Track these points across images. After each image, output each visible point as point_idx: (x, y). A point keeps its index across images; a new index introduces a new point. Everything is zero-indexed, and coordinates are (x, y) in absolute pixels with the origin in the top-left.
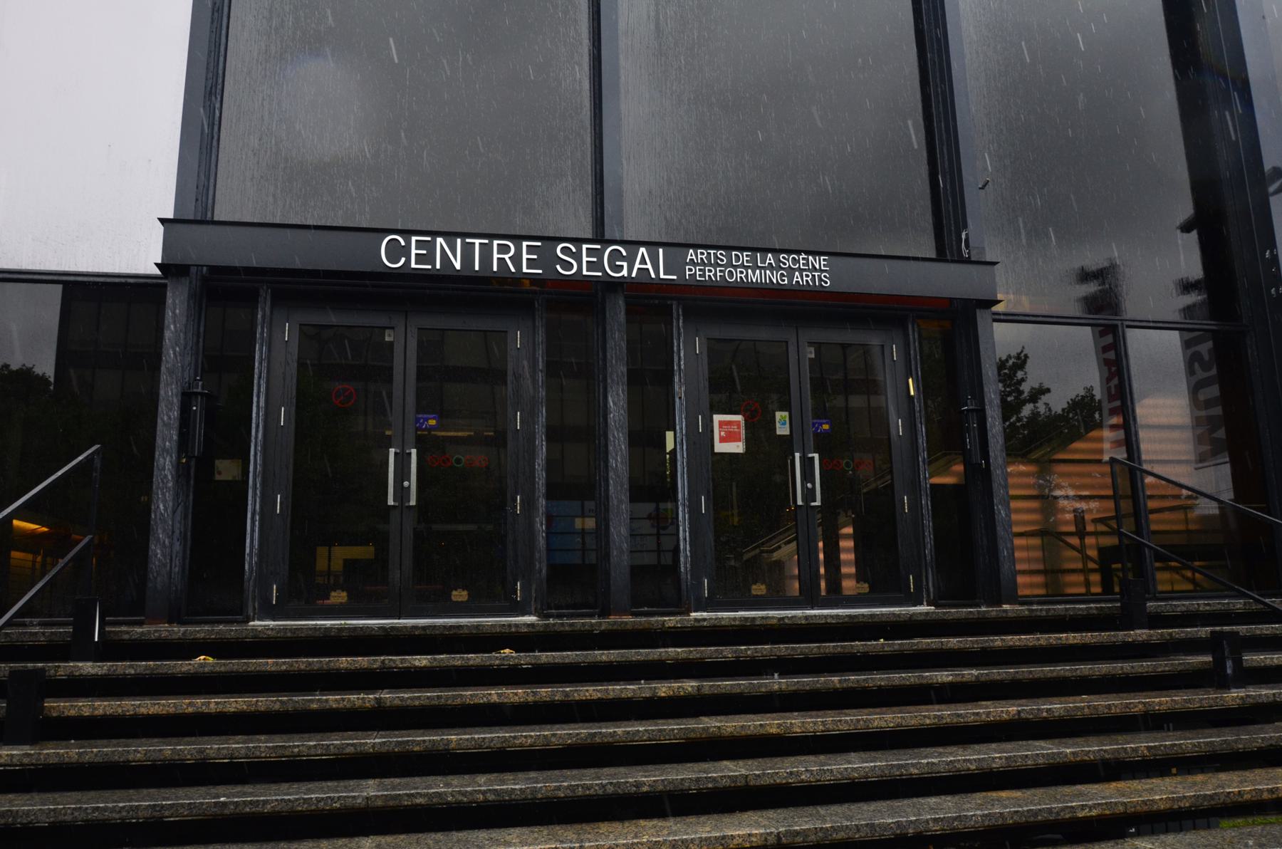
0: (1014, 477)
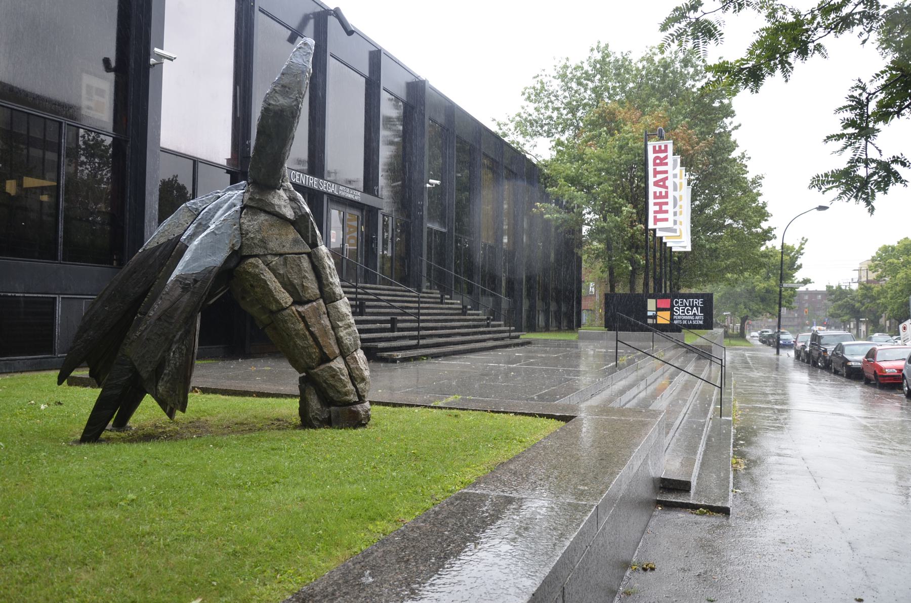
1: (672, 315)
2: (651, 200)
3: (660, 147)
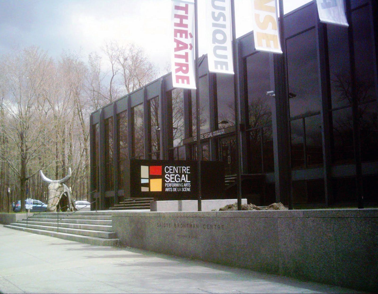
1: (164, 183)
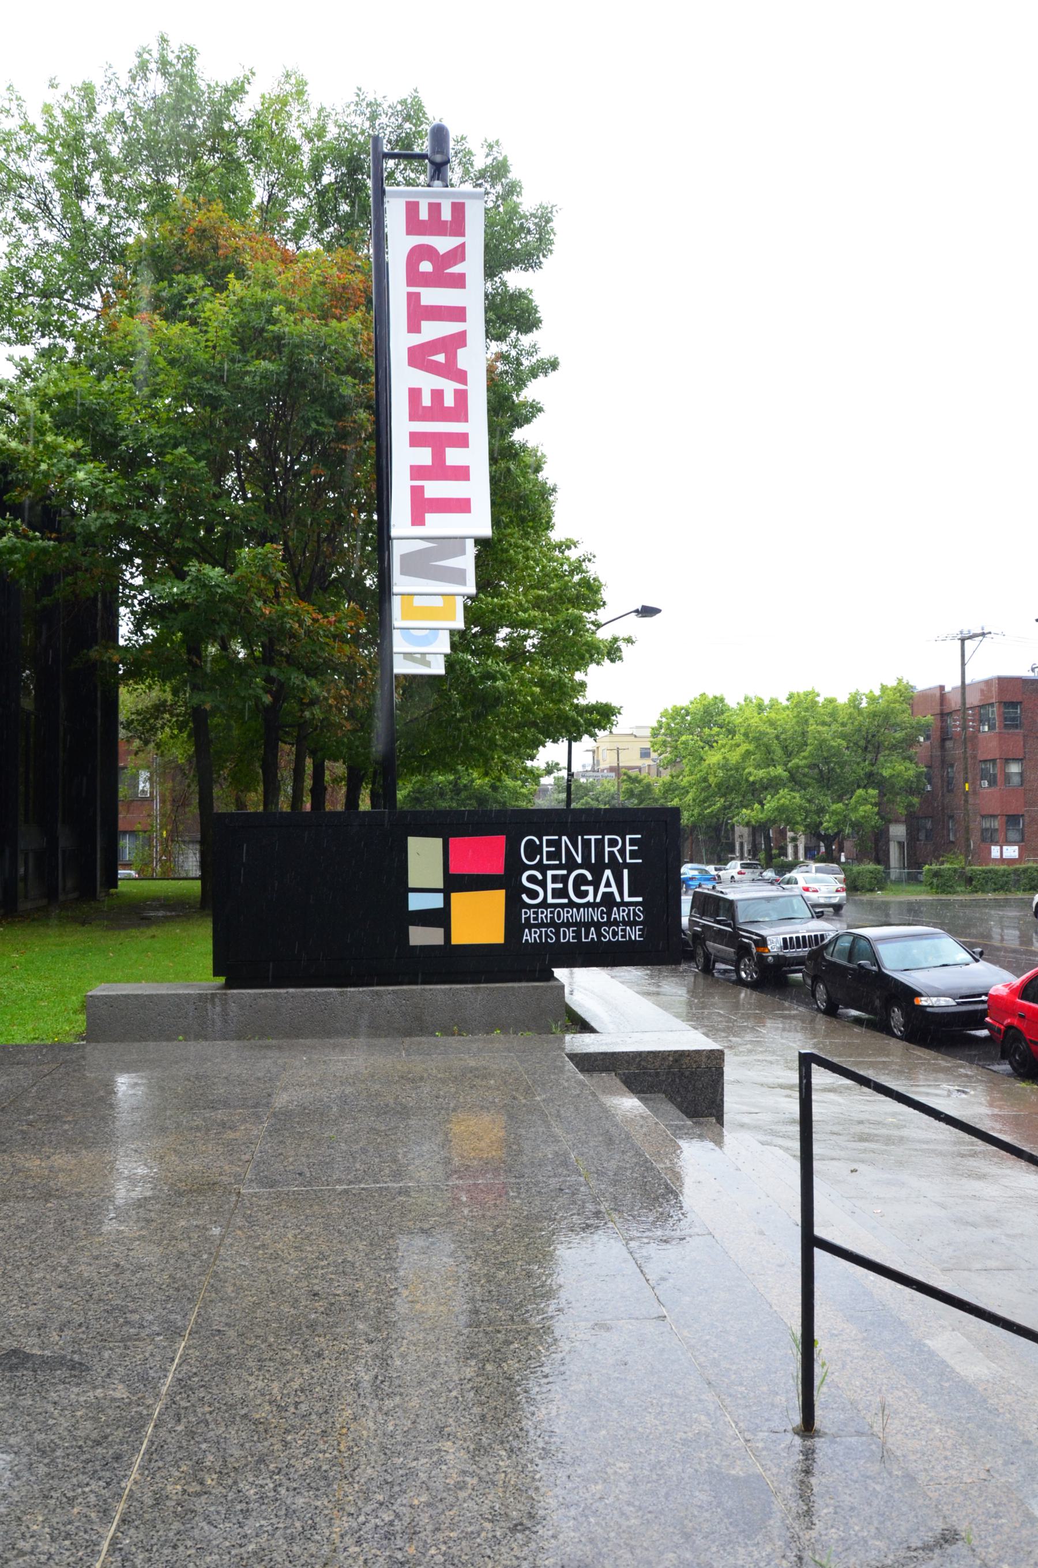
0: (1005, 944)
1: (513, 906)
2: (401, 425)
3: (435, 209)
